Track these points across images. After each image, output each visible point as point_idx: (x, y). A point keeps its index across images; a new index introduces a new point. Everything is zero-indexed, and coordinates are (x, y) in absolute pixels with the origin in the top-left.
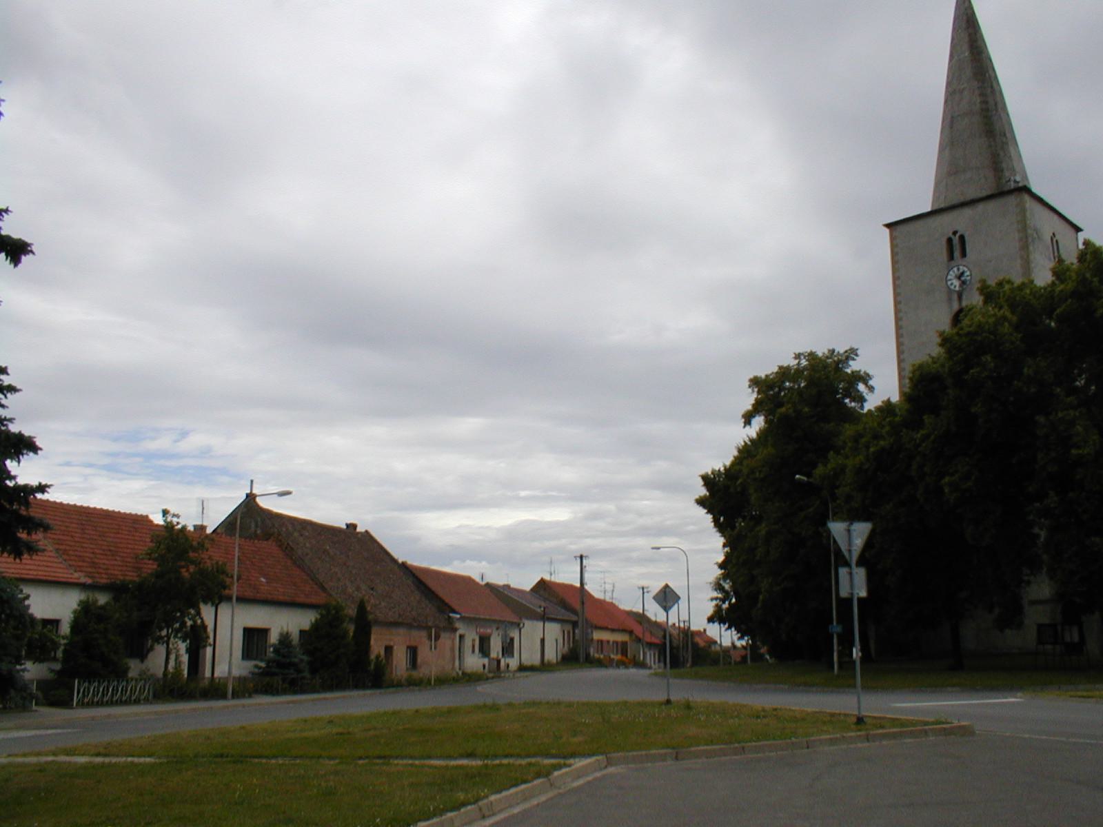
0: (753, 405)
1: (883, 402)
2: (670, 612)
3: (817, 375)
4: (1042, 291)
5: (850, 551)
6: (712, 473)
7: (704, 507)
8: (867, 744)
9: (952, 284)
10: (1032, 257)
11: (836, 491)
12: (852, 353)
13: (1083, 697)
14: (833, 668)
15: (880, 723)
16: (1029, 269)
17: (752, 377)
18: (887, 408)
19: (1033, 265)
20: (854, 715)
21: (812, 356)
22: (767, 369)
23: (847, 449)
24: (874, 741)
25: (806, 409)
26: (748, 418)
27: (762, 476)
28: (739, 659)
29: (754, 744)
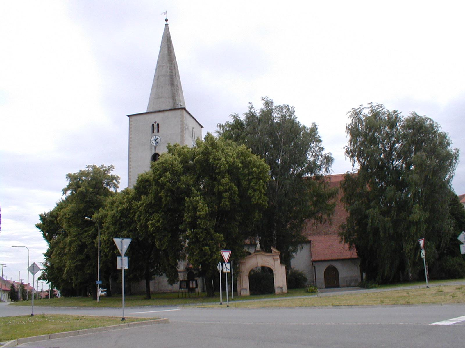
0: (68, 186)
1: (125, 189)
2: (35, 275)
3: (96, 176)
4: (190, 150)
5: (122, 250)
6: (45, 214)
7: (40, 228)
8: (129, 328)
9: (152, 143)
10: (184, 135)
11: (103, 225)
12: (111, 167)
13: (202, 308)
14: (97, 299)
15: (132, 320)
16: (183, 140)
17: (68, 174)
18: (126, 192)
19: (185, 139)
20: (121, 318)
21: (94, 167)
22: (75, 171)
23: (108, 207)
24: (131, 327)
25: (91, 189)
26: (65, 191)
27: (69, 216)
28: (45, 297)
29: (83, 330)
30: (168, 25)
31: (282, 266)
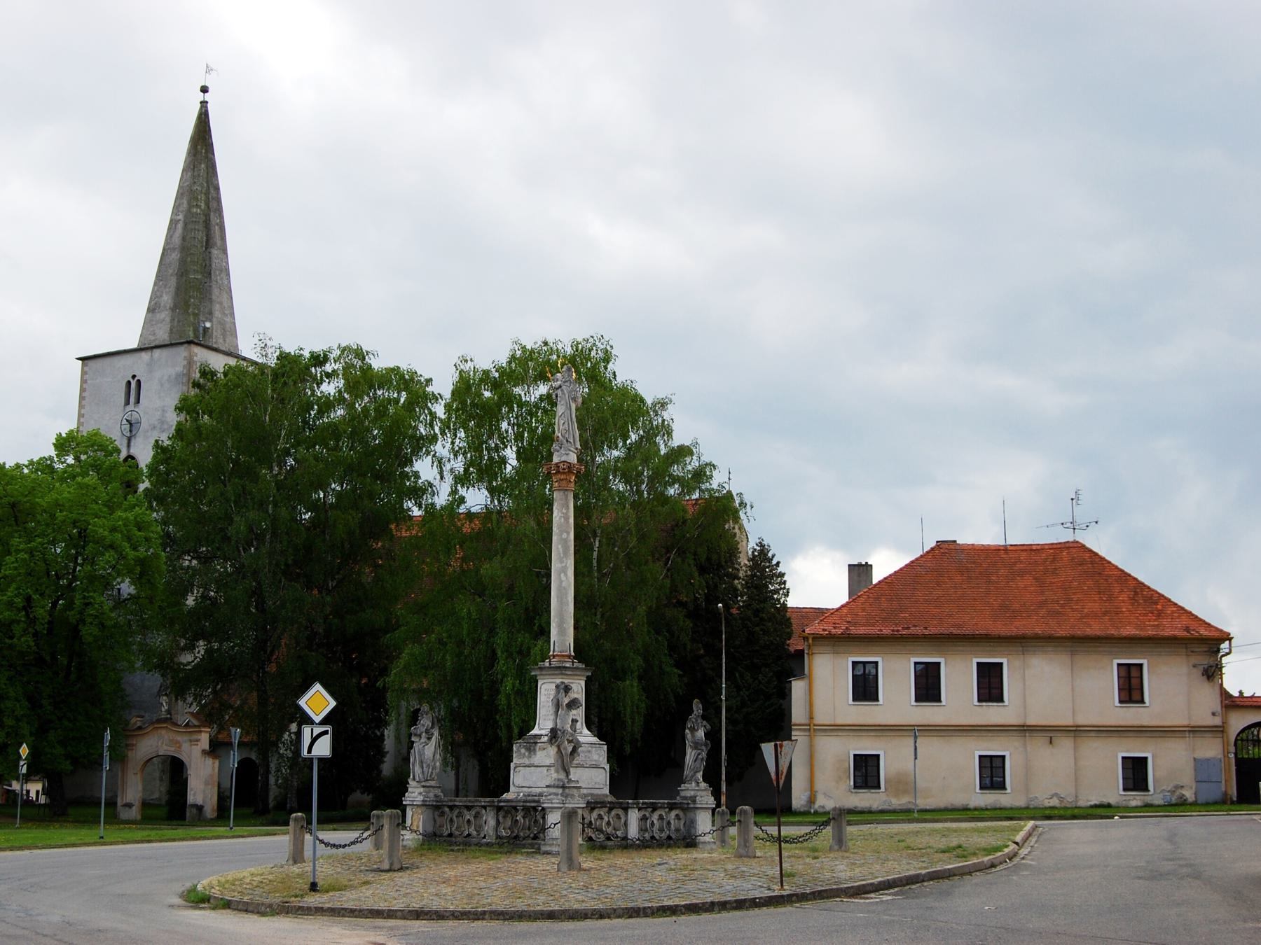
30: (207, 102)
31: (207, 758)
